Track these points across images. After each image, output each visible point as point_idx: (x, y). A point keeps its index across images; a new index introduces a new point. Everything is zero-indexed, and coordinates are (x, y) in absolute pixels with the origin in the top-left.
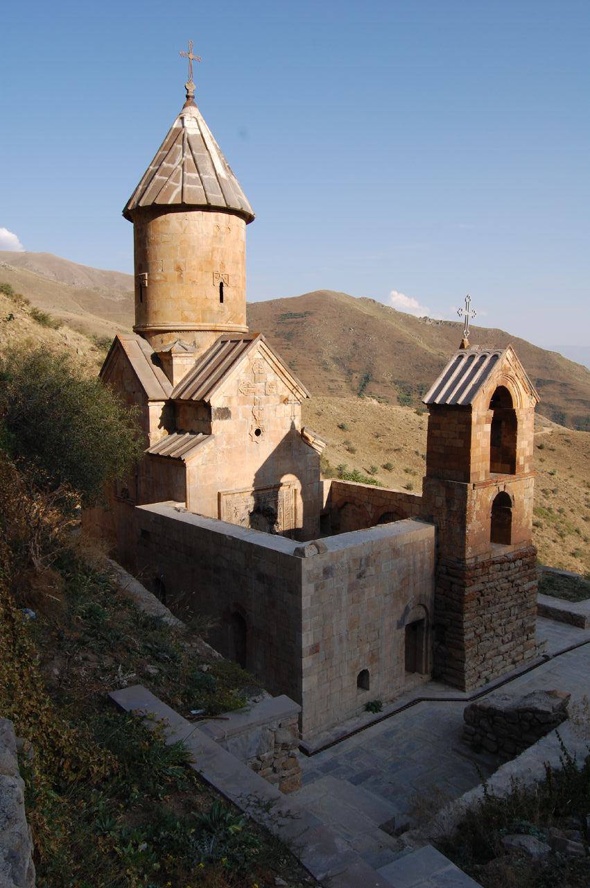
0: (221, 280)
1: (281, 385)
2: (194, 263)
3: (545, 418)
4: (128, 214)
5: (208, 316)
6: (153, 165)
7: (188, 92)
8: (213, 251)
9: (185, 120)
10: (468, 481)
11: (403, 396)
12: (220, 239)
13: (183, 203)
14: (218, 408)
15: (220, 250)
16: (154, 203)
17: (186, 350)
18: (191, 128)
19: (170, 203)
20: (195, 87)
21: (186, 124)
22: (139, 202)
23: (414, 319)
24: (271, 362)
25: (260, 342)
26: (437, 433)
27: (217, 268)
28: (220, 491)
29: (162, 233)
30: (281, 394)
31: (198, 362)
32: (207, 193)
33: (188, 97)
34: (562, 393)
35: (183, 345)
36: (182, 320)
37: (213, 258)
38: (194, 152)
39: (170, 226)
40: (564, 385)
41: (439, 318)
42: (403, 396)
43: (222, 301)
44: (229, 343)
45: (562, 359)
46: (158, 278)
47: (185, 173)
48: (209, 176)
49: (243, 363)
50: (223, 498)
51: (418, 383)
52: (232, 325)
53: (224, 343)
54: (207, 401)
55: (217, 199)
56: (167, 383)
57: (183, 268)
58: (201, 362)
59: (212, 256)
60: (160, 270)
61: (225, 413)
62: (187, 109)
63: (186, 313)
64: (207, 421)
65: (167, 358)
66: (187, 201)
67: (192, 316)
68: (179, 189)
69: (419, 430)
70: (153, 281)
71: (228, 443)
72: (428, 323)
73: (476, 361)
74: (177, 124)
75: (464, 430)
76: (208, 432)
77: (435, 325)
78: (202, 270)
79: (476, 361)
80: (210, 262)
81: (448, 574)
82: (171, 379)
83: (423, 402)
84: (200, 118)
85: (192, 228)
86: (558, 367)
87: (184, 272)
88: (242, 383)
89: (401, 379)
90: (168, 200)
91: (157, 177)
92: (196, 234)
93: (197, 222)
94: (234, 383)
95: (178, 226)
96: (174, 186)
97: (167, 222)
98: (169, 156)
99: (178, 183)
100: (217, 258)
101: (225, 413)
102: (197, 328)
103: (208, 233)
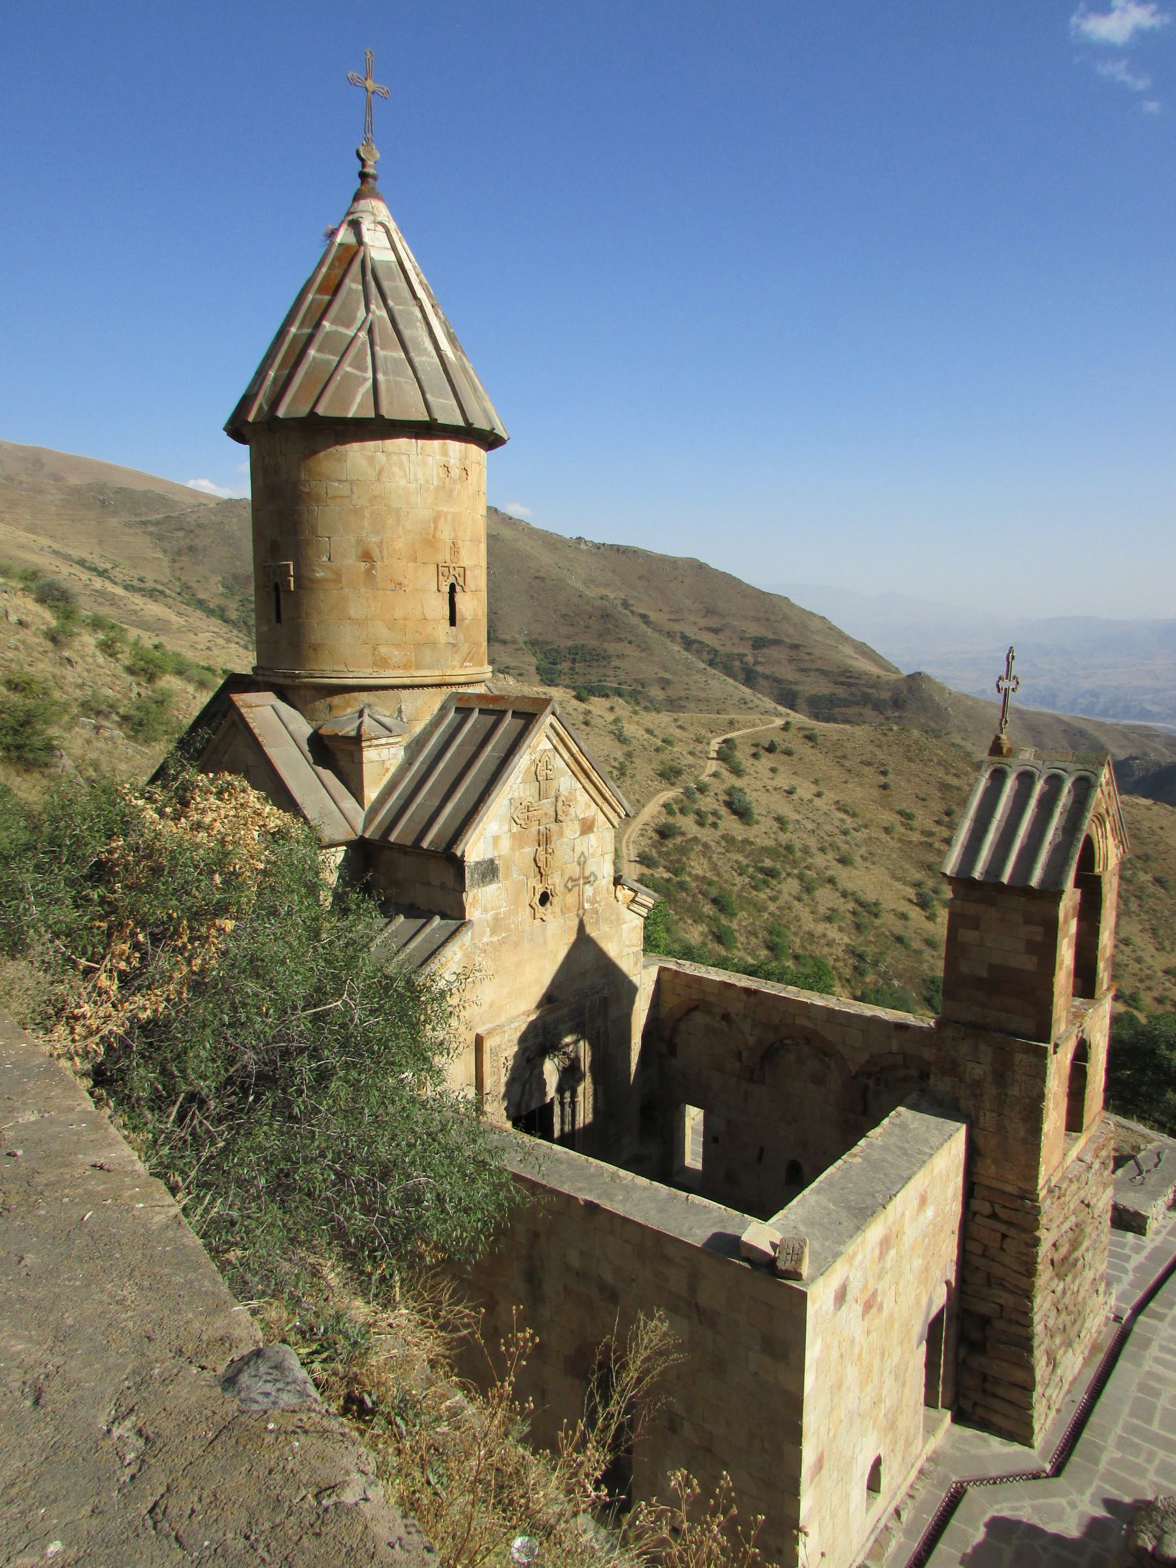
0: (452, 580)
1: (582, 797)
2: (400, 544)
3: (765, 699)
4: (237, 429)
5: (428, 655)
6: (297, 323)
7: (364, 166)
8: (436, 520)
9: (364, 228)
10: (1047, 1039)
11: (544, 664)
12: (451, 492)
13: (379, 417)
14: (477, 863)
15: (449, 517)
16: (312, 414)
17: (390, 731)
18: (377, 247)
19: (350, 416)
20: (378, 155)
21: (367, 237)
22: (275, 402)
23: (560, 539)
24: (566, 755)
25: (550, 719)
26: (968, 935)
27: (445, 555)
28: (480, 1030)
29: (329, 478)
30: (582, 816)
31: (414, 748)
32: (429, 396)
33: (363, 176)
34: (791, 661)
35: (377, 717)
36: (375, 664)
37: (438, 535)
38: (391, 303)
39: (349, 464)
40: (795, 647)
41: (598, 540)
42: (544, 664)
43: (453, 622)
44: (476, 714)
45: (792, 605)
46: (320, 575)
47: (377, 348)
48: (427, 360)
49: (523, 762)
50: (488, 1045)
51: (570, 643)
52: (459, 671)
53: (464, 712)
54: (459, 854)
55: (449, 415)
56: (349, 803)
57: (376, 553)
58: (419, 752)
59: (436, 528)
60: (325, 559)
61: (489, 871)
62: (363, 204)
63: (383, 650)
64: (454, 890)
65: (350, 748)
66: (388, 412)
67: (396, 655)
68: (369, 383)
69: (583, 727)
70: (310, 579)
71: (493, 932)
72: (583, 546)
73: (1039, 787)
74: (344, 235)
75: (1039, 938)
76: (456, 914)
77: (594, 551)
78: (415, 561)
79: (1039, 787)
80: (431, 543)
81: (993, 1216)
82: (358, 794)
83: (944, 875)
84: (392, 226)
85: (395, 469)
86: (786, 618)
87: (378, 564)
88: (518, 802)
89: (540, 639)
90: (348, 409)
91: (312, 352)
92: (403, 482)
93: (404, 458)
94: (506, 802)
95: (363, 463)
96: (356, 377)
97: (342, 459)
98: (336, 307)
99: (365, 370)
100: (445, 535)
101: (489, 871)
102: (407, 681)
103: (427, 481)
